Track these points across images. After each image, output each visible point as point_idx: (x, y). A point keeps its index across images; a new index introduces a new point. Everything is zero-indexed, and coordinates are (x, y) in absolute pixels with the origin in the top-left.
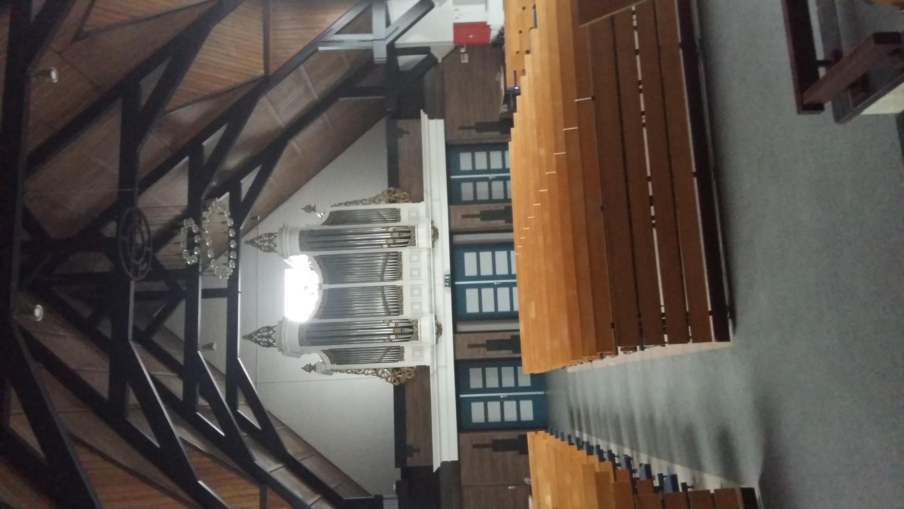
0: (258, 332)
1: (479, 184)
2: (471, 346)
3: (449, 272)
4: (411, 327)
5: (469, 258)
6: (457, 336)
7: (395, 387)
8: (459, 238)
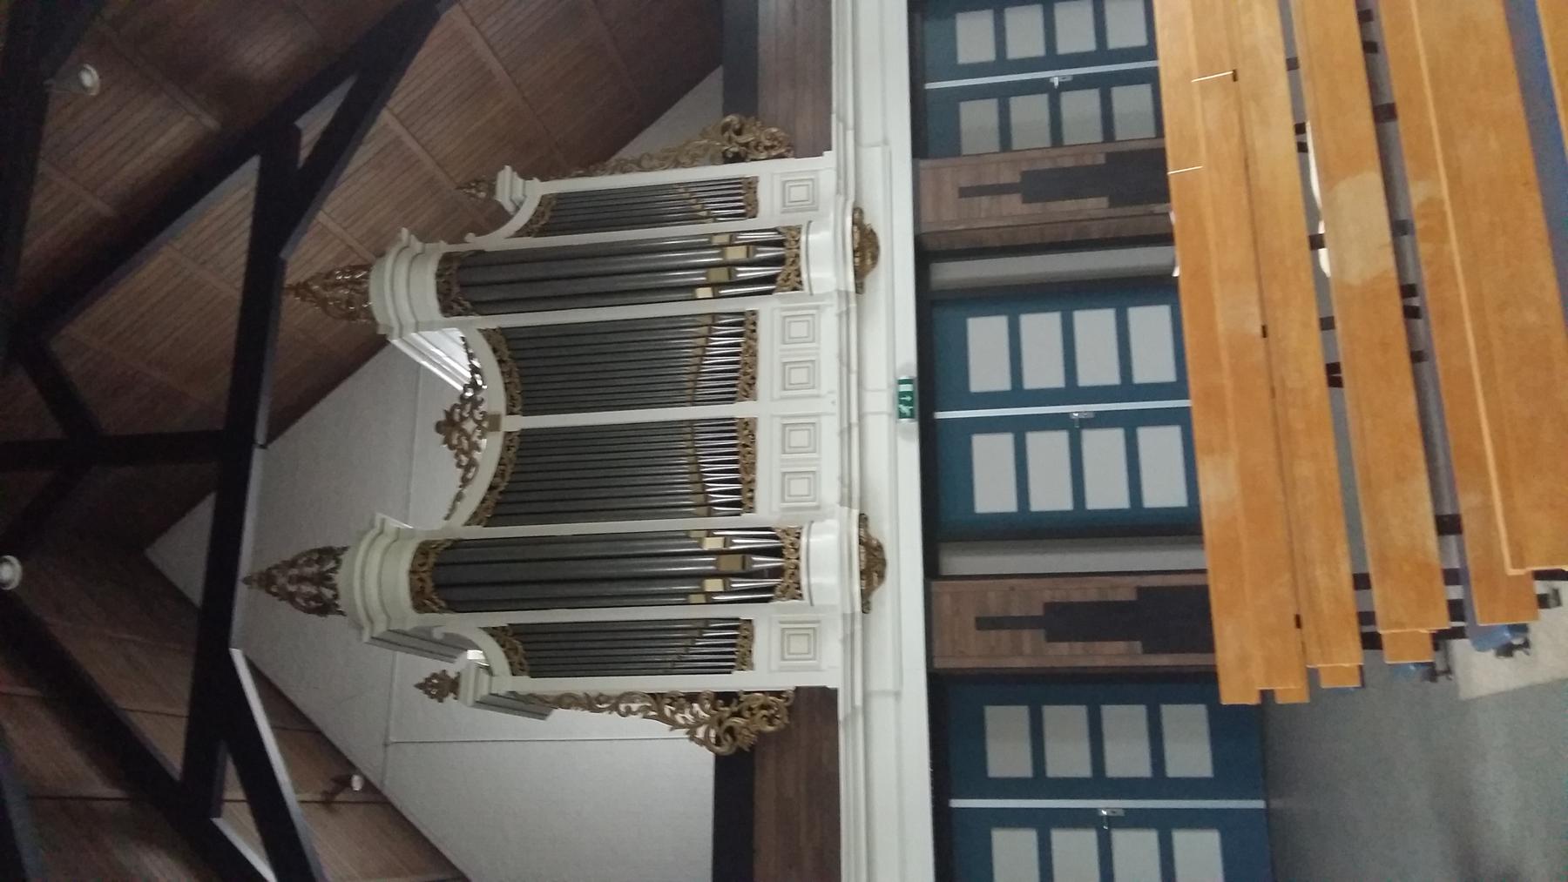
0: (293, 564)
1: (1018, 104)
2: (984, 623)
3: (913, 373)
4: (776, 552)
5: (985, 337)
6: (935, 585)
7: (720, 761)
8: (951, 273)
